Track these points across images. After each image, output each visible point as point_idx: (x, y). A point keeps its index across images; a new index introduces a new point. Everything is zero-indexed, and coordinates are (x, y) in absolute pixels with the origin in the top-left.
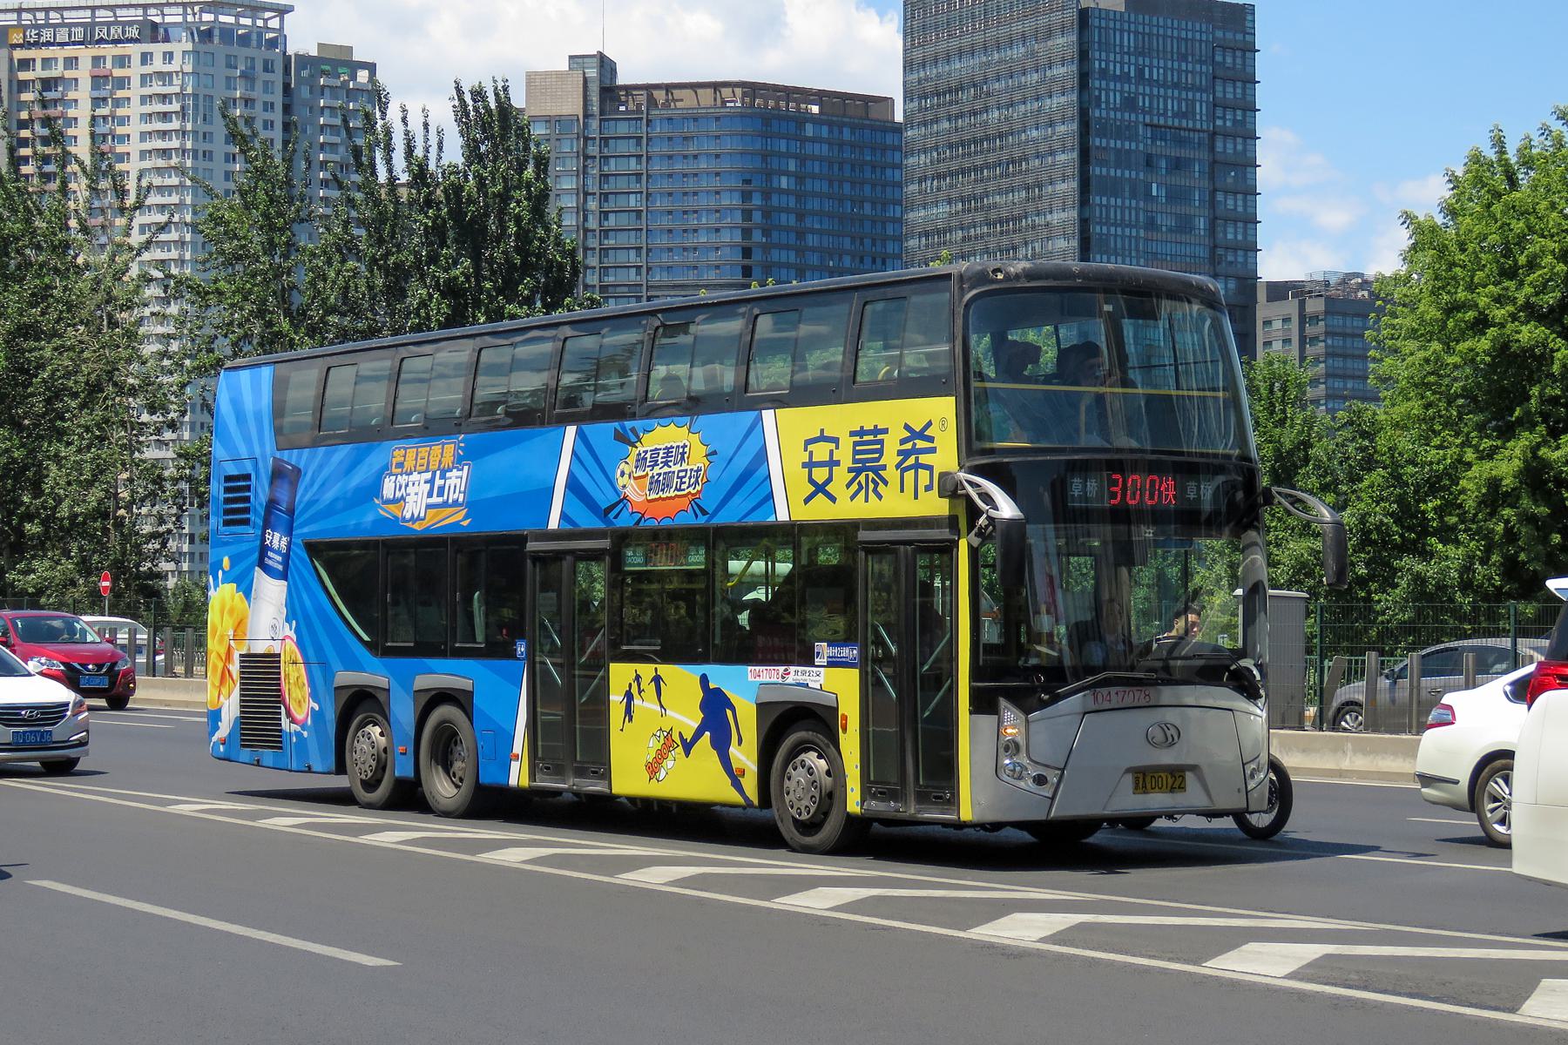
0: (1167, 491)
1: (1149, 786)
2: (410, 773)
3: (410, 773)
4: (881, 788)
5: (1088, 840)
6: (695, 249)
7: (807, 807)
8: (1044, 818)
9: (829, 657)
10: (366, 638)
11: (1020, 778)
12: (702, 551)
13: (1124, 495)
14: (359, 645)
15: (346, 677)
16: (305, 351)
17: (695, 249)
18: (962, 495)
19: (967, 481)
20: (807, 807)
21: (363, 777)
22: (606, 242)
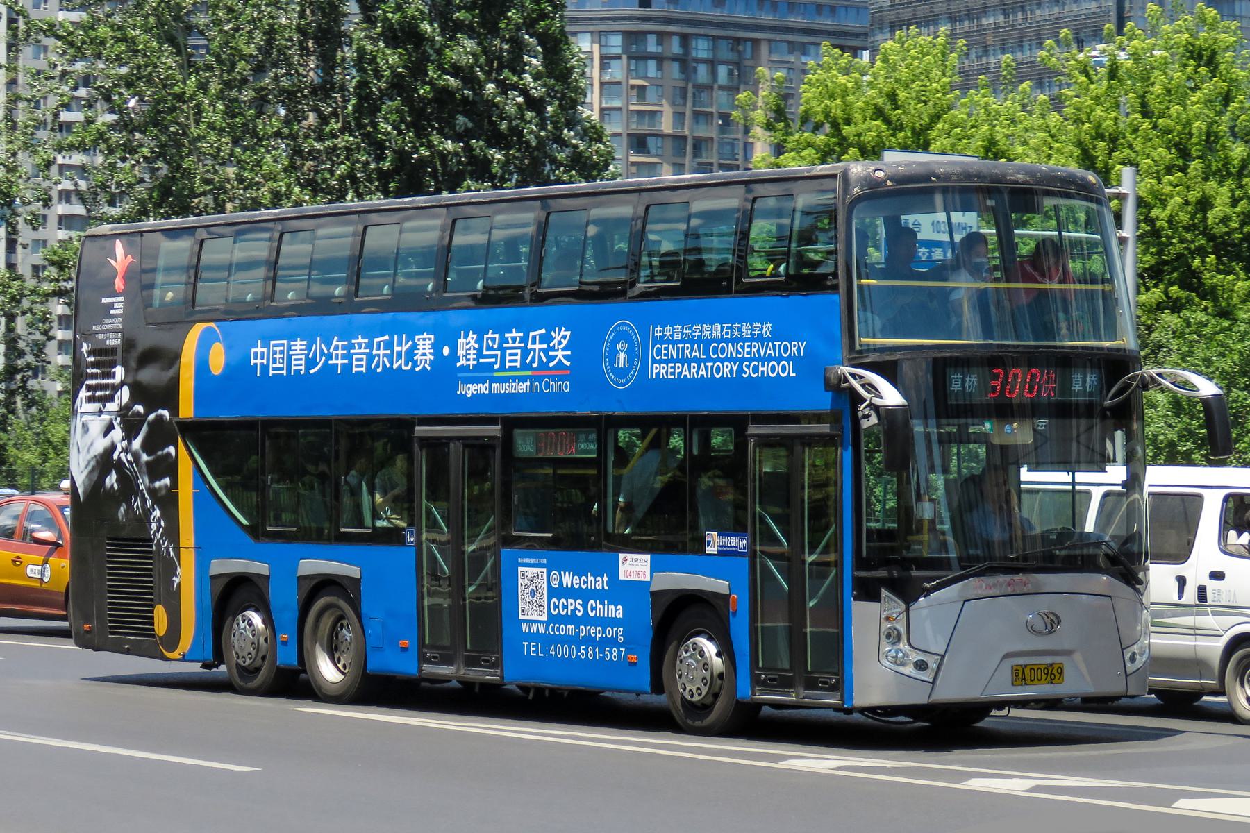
0: (1044, 384)
1: (1028, 677)
2: (293, 661)
3: (293, 661)
4: (773, 675)
5: (979, 724)
7: (698, 689)
8: (924, 701)
9: (719, 546)
10: (245, 522)
11: (903, 664)
12: (593, 436)
13: (1003, 389)
14: (237, 528)
15: (221, 567)
16: (509, 192)
18: (845, 389)
19: (850, 374)
20: (698, 689)
21: (241, 661)
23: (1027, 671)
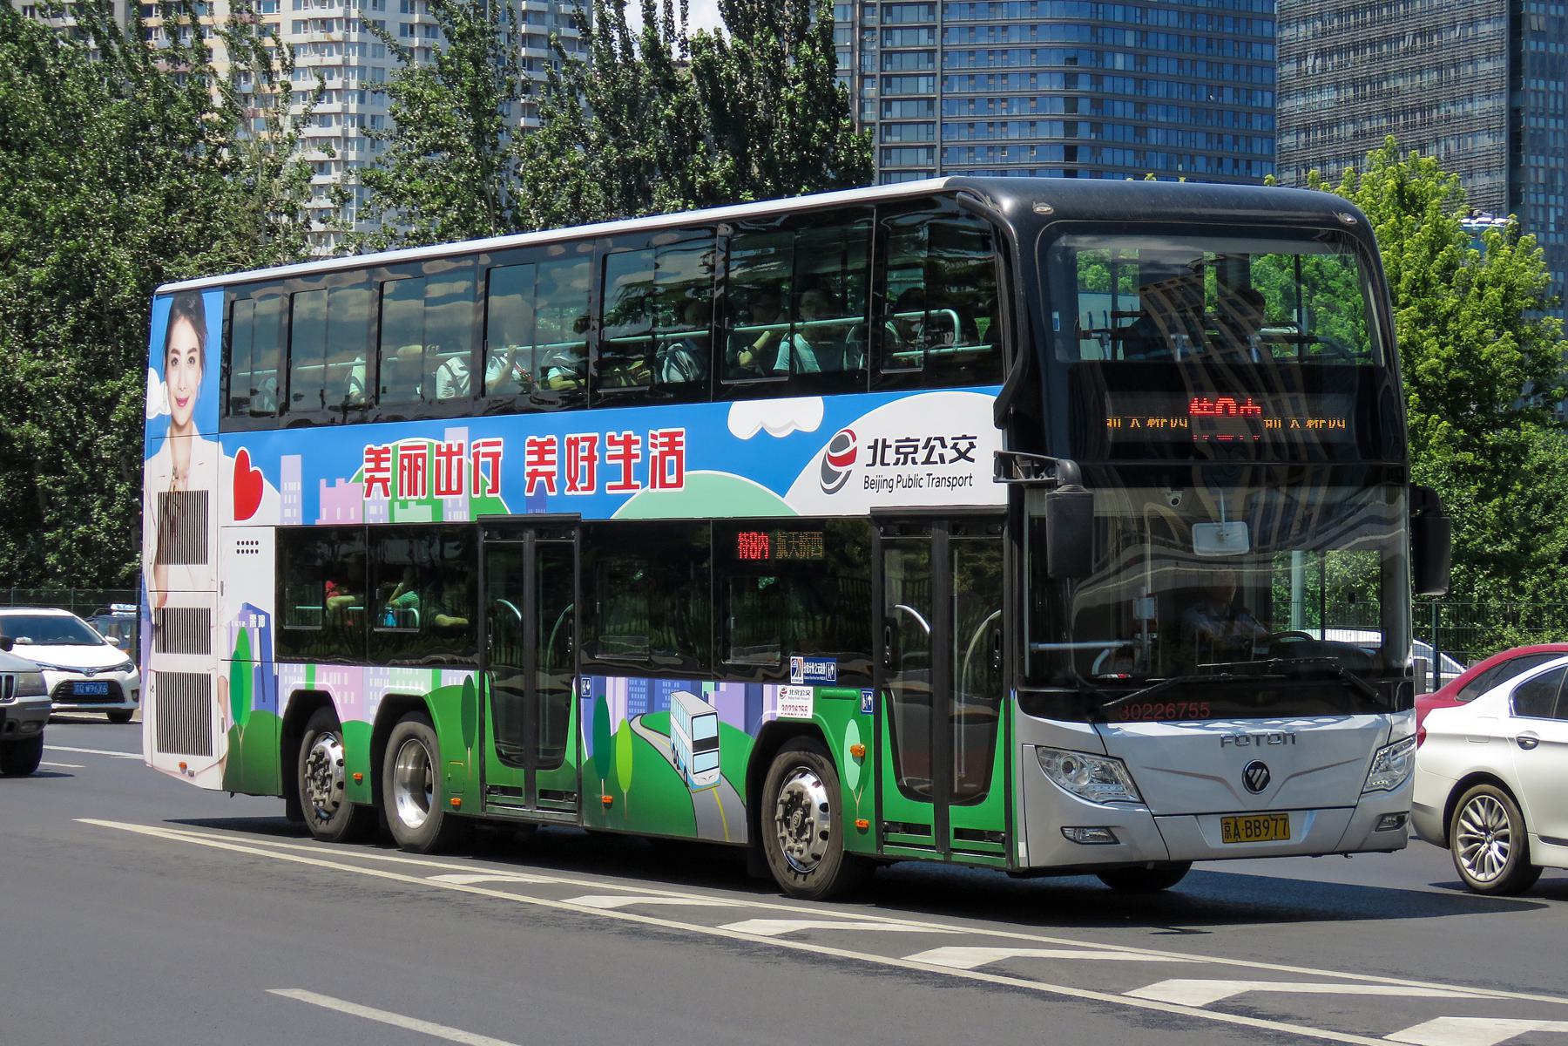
1: (1243, 834)
5: (1170, 889)
6: (1004, 148)
17: (1004, 148)
22: (888, 139)
23: (1241, 825)
